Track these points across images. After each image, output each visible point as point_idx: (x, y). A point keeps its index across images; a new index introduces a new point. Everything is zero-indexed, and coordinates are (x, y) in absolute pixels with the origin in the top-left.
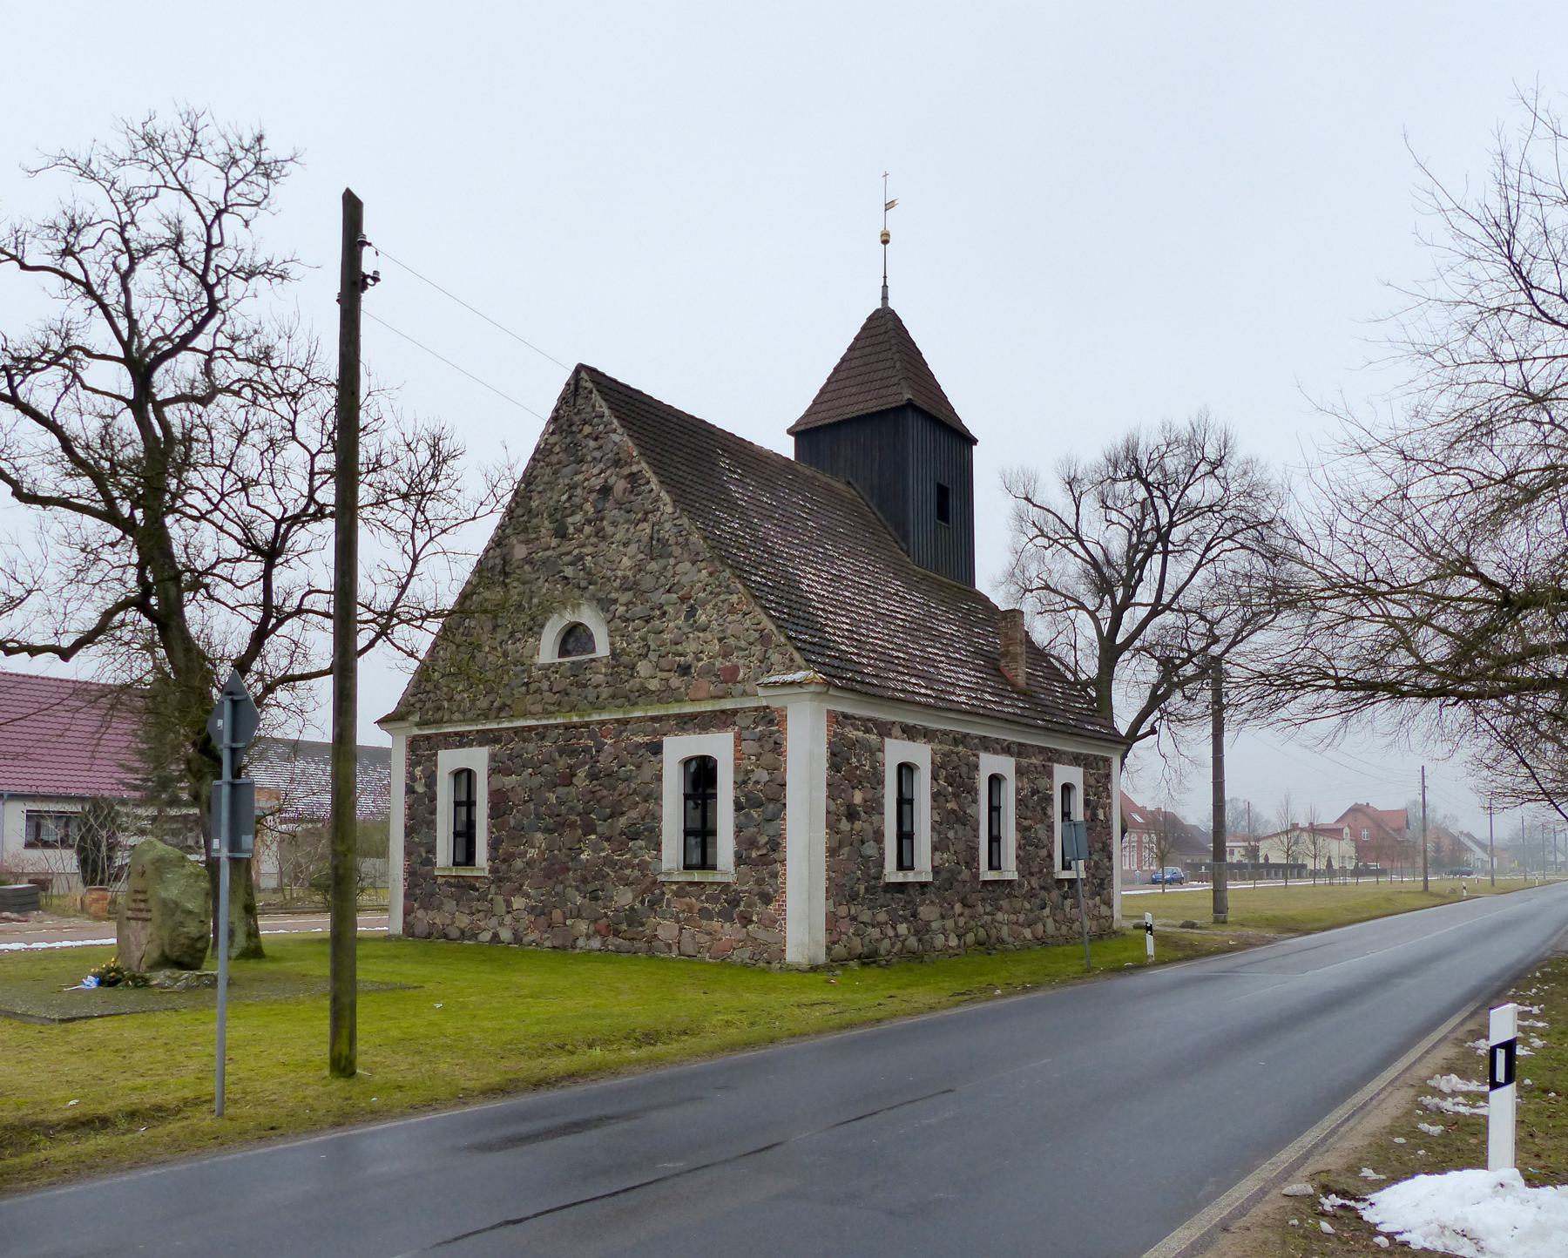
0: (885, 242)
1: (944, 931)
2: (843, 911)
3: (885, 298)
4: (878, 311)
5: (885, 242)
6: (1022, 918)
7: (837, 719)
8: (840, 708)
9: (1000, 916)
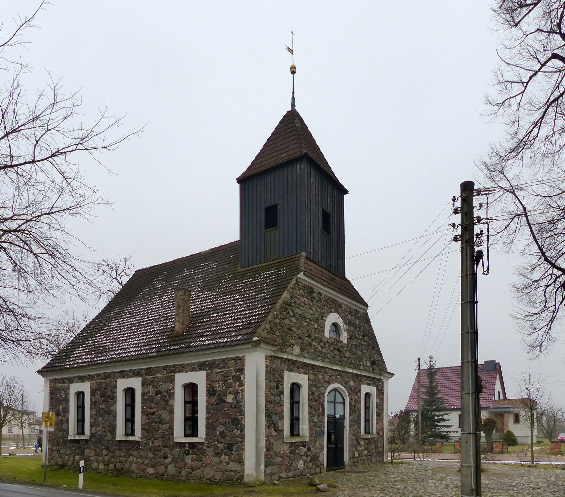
0: (293, 73)
1: (97, 461)
2: (54, 448)
3: (293, 105)
4: (289, 112)
5: (293, 73)
6: (146, 461)
7: (51, 381)
8: (54, 378)
9: (131, 459)
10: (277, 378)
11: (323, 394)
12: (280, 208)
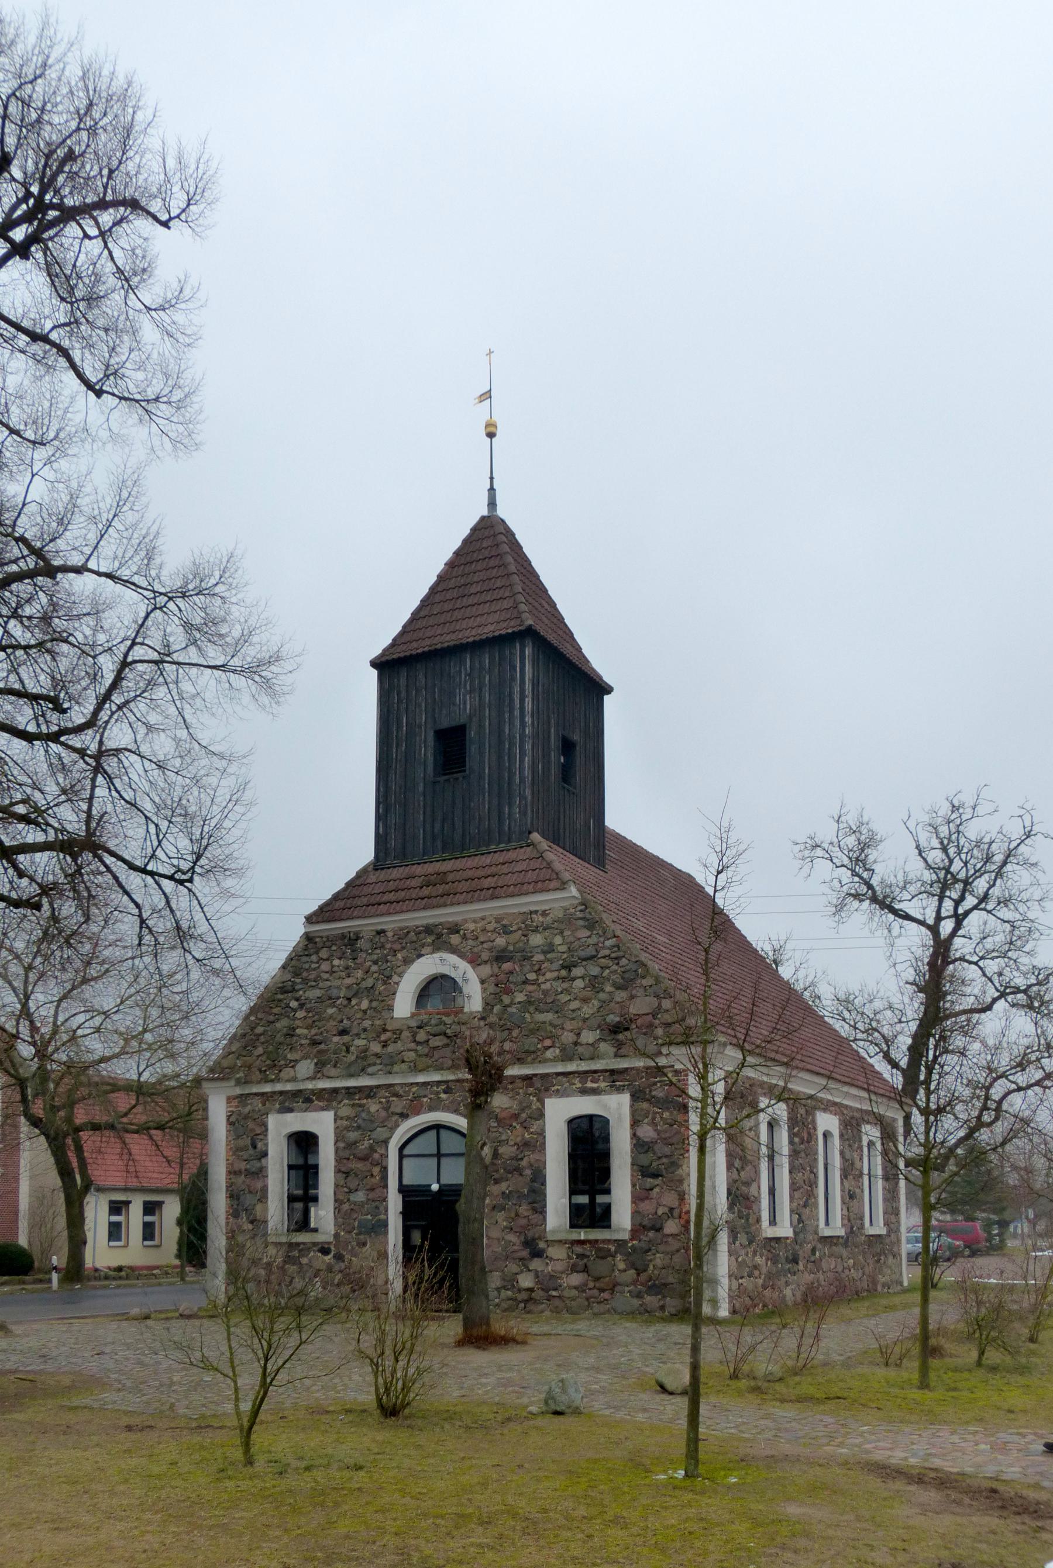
0: (491, 435)
3: (492, 504)
4: (483, 518)
5: (491, 435)
10: (252, 1130)
11: (386, 1142)
12: (472, 733)
